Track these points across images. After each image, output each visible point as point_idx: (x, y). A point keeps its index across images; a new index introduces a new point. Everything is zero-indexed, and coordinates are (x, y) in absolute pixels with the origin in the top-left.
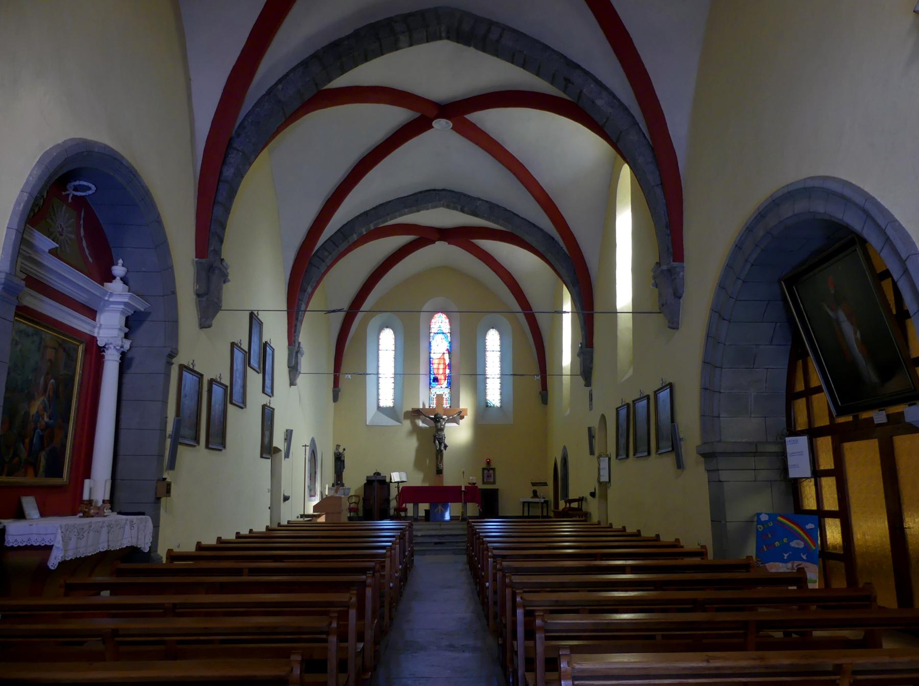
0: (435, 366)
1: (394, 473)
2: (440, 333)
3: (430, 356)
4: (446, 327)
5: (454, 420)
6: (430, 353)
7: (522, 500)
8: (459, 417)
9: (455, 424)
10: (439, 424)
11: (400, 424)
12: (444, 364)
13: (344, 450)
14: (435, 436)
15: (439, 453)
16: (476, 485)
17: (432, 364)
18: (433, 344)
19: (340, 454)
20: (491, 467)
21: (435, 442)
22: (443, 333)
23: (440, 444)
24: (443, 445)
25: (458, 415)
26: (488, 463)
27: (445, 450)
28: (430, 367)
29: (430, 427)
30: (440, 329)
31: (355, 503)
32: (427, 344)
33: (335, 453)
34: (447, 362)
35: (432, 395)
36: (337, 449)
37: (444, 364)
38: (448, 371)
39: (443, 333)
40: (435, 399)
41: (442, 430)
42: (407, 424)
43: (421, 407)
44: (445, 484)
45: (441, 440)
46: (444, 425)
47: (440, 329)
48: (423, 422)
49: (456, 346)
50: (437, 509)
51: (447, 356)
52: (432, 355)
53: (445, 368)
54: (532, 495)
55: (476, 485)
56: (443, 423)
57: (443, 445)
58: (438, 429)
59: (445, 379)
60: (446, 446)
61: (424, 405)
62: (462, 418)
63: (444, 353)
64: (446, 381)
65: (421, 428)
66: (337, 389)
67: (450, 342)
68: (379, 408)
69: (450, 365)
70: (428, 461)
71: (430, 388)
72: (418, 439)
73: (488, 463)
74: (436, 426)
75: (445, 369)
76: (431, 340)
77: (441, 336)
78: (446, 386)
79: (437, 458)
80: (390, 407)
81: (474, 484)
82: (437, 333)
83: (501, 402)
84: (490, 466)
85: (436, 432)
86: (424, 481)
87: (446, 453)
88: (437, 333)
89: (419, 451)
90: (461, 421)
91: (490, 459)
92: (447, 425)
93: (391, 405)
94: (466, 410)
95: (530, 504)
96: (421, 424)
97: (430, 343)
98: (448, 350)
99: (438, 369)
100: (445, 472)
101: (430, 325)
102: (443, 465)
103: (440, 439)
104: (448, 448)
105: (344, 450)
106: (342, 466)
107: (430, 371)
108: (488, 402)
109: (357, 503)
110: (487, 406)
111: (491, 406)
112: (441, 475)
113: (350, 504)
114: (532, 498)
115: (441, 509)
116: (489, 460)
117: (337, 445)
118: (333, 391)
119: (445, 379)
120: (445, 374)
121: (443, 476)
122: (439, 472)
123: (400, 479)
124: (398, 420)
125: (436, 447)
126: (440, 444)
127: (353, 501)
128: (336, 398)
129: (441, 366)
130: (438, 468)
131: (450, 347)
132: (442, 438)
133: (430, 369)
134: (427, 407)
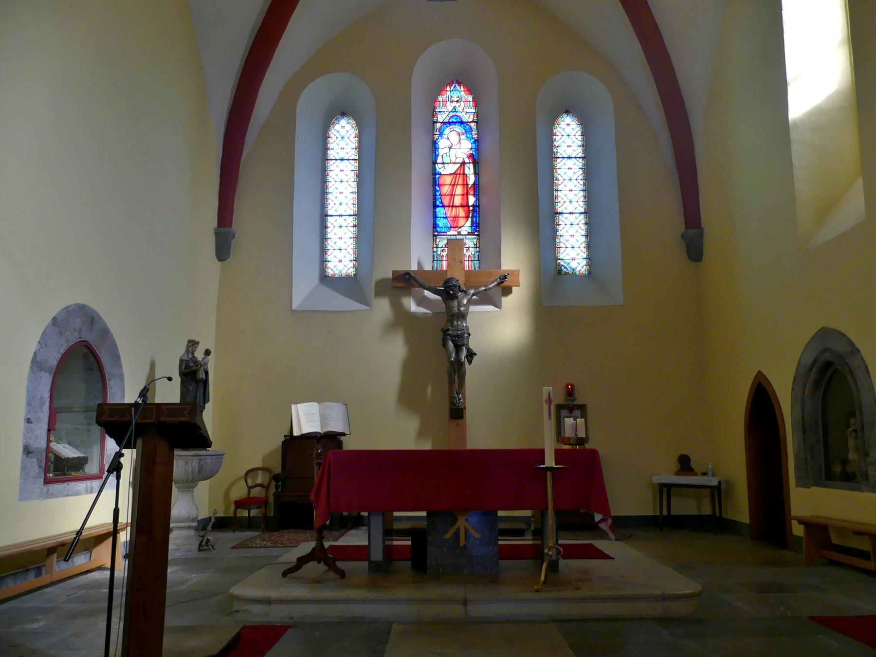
0: (446, 189)
1: (301, 407)
2: (455, 123)
3: (435, 169)
4: (467, 112)
5: (486, 298)
6: (435, 163)
7: (657, 480)
8: (499, 289)
9: (490, 308)
10: (455, 303)
11: (368, 308)
12: (465, 184)
13: (207, 353)
14: (445, 332)
15: (456, 370)
16: (588, 446)
17: (439, 185)
18: (442, 143)
19: (196, 362)
20: (575, 403)
21: (444, 345)
22: (462, 123)
23: (458, 348)
24: (464, 352)
25: (499, 284)
26: (570, 393)
27: (470, 362)
28: (435, 191)
29: (433, 313)
30: (455, 113)
31: (261, 485)
32: (428, 144)
33: (181, 361)
34: (471, 180)
35: (439, 250)
36: (187, 351)
37: (465, 184)
38: (472, 200)
39: (462, 123)
40: (444, 259)
41: (463, 316)
42: (383, 307)
43: (414, 267)
44: (470, 446)
45: (459, 340)
46: (467, 310)
47: (455, 113)
48: (419, 304)
49: (491, 147)
50: (453, 530)
51: (470, 170)
52: (438, 167)
53: (467, 194)
54: (676, 467)
55: (588, 446)
56: (465, 301)
57: (464, 352)
58: (453, 315)
59: (467, 217)
60: (471, 355)
61: (419, 264)
62: (507, 291)
63: (463, 164)
64: (470, 219)
65: (414, 316)
66: (224, 230)
67: (476, 141)
68: (324, 277)
69: (475, 186)
70: (429, 390)
71: (434, 235)
72: (408, 340)
73: (570, 393)
74: (449, 308)
75: (465, 195)
76: (436, 137)
77: (458, 128)
78: (469, 230)
79: (451, 383)
80: (348, 277)
81: (581, 441)
82: (449, 123)
83: (588, 264)
84: (574, 400)
85: (448, 321)
86: (421, 434)
87: (470, 370)
88: (449, 123)
89: (409, 368)
90: (506, 301)
91: (573, 383)
92: (473, 308)
93: (351, 271)
94: (516, 273)
95: (673, 490)
96: (413, 307)
97: (435, 143)
98: (471, 156)
99: (452, 195)
100: (469, 414)
101: (435, 108)
102: (464, 397)
103: (458, 336)
104: (475, 358)
105: (207, 353)
106: (200, 395)
107: (435, 200)
108: (562, 263)
109: (266, 487)
110: (559, 272)
111: (567, 273)
112: (459, 421)
113: (250, 488)
114: (678, 473)
115: (466, 530)
116: (572, 385)
117: (190, 341)
118: (217, 234)
119: (467, 217)
120: (467, 185)
121: (465, 422)
122: (457, 413)
123: (323, 424)
124: (363, 300)
125: (449, 356)
126: (458, 348)
127: (259, 481)
128: (223, 251)
129: (459, 190)
130: (452, 404)
131: (477, 150)
132: (463, 334)
133: (435, 195)
134: (428, 267)
